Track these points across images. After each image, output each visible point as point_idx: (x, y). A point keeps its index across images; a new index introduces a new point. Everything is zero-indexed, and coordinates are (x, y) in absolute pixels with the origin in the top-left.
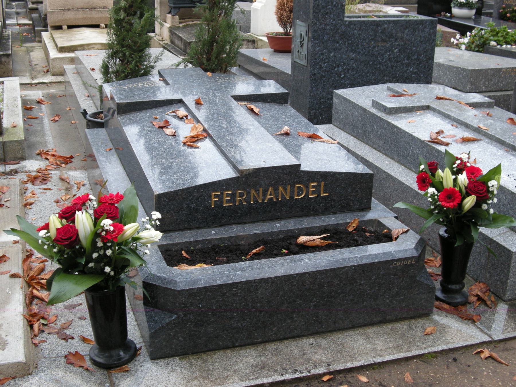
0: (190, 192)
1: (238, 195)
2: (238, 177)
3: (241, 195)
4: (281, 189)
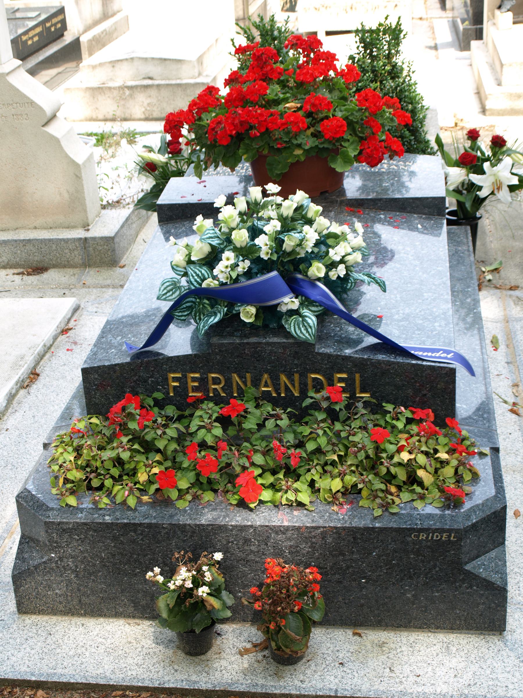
0: (133, 370)
1: (210, 382)
2: (195, 355)
3: (216, 381)
4: (283, 378)
